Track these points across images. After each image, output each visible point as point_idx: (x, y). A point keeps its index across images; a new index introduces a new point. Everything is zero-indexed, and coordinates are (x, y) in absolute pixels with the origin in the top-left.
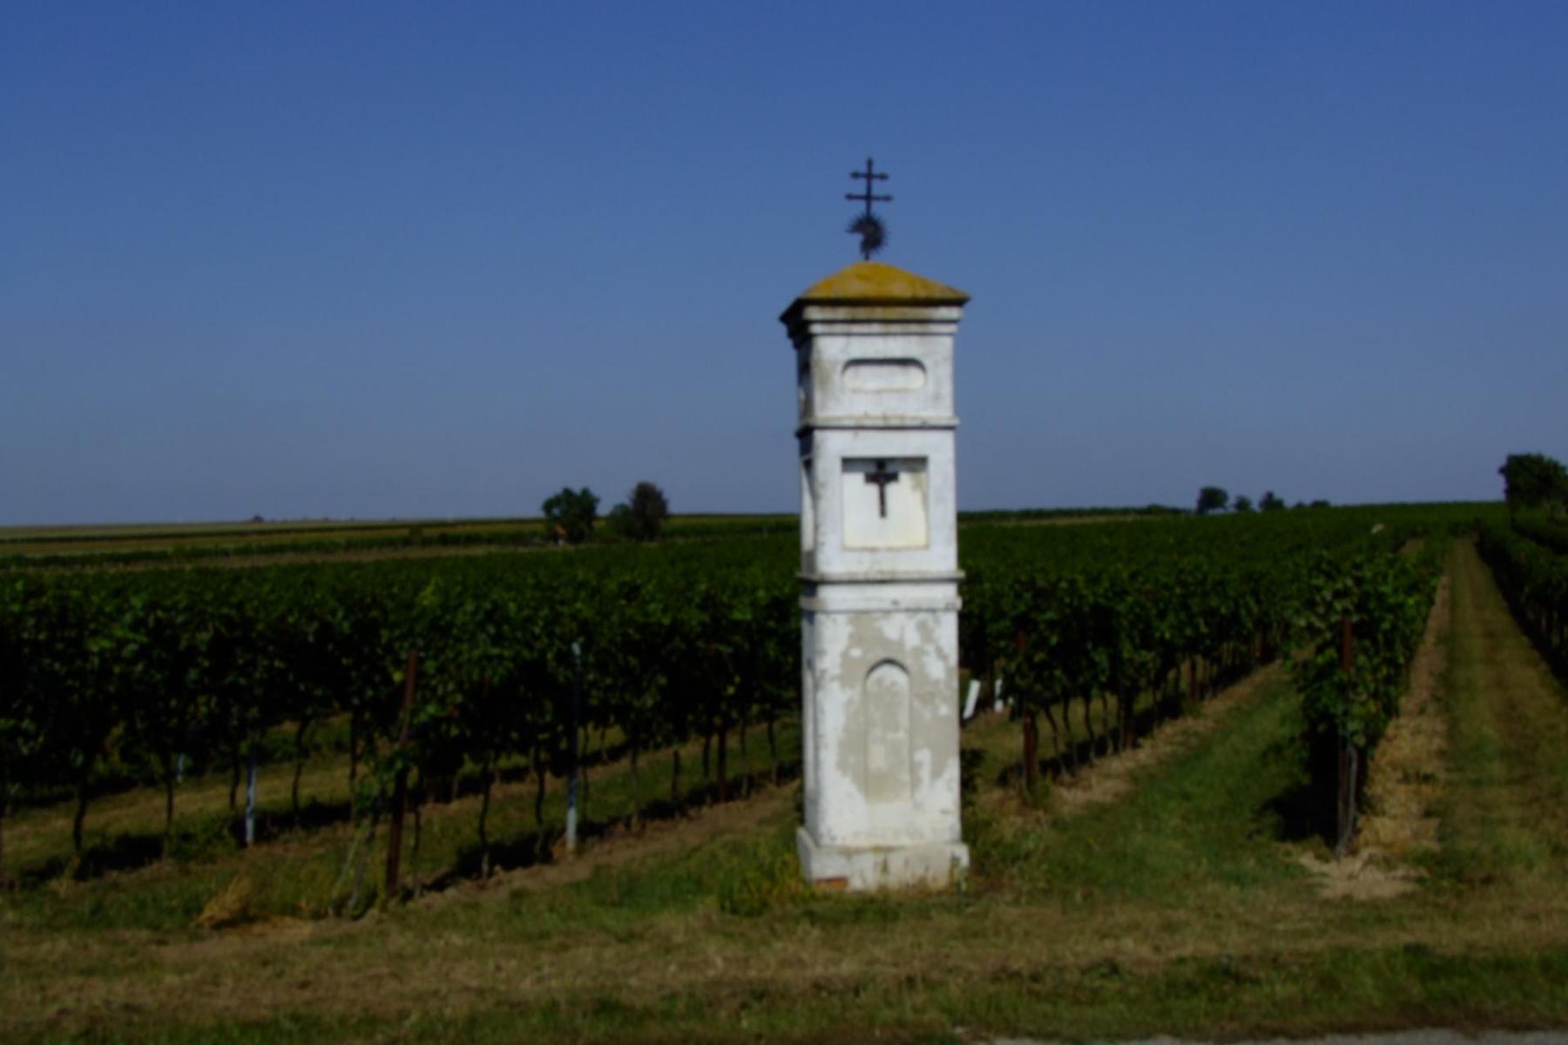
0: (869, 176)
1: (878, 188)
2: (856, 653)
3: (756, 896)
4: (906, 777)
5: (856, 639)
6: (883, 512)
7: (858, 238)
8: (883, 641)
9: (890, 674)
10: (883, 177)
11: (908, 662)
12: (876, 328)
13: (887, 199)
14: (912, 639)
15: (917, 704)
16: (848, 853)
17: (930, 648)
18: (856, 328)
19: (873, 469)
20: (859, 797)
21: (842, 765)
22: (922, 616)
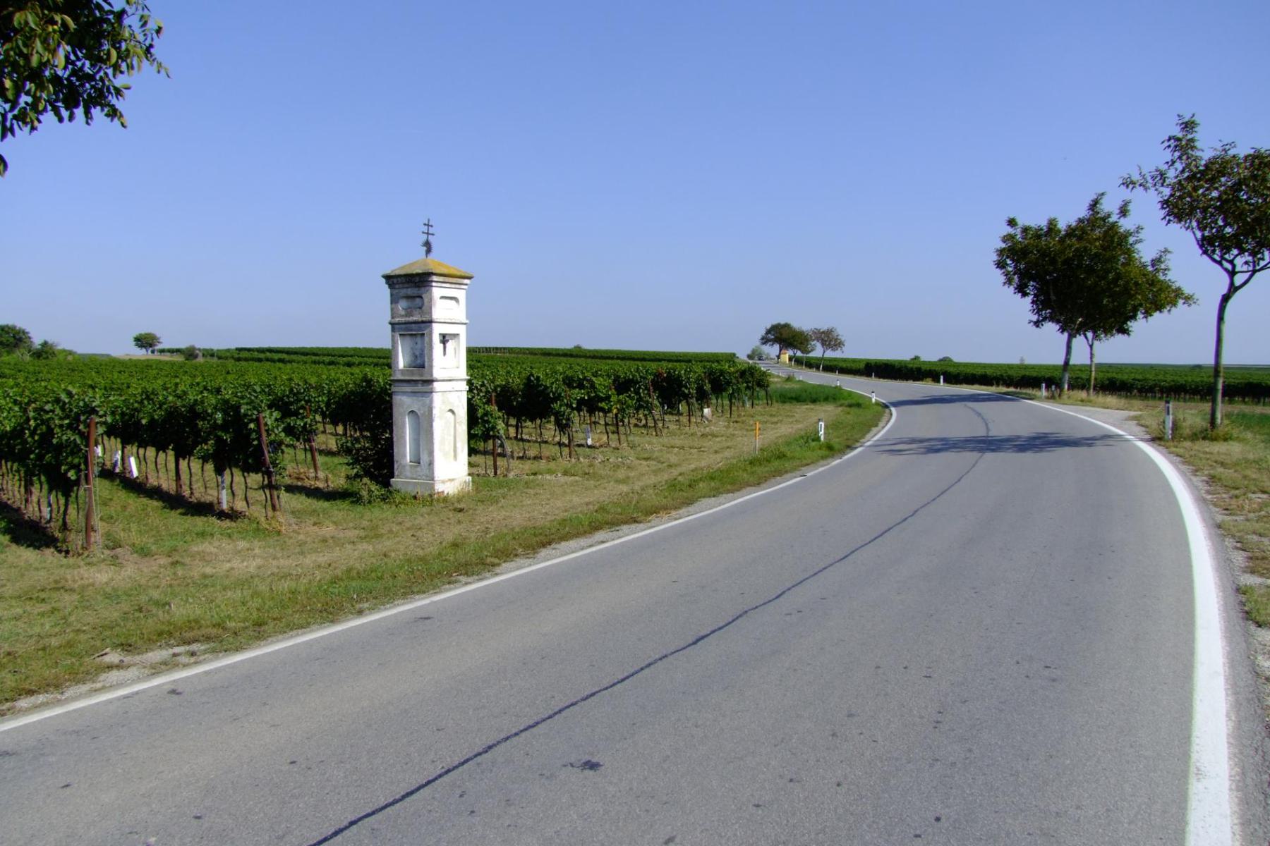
7: (425, 248)
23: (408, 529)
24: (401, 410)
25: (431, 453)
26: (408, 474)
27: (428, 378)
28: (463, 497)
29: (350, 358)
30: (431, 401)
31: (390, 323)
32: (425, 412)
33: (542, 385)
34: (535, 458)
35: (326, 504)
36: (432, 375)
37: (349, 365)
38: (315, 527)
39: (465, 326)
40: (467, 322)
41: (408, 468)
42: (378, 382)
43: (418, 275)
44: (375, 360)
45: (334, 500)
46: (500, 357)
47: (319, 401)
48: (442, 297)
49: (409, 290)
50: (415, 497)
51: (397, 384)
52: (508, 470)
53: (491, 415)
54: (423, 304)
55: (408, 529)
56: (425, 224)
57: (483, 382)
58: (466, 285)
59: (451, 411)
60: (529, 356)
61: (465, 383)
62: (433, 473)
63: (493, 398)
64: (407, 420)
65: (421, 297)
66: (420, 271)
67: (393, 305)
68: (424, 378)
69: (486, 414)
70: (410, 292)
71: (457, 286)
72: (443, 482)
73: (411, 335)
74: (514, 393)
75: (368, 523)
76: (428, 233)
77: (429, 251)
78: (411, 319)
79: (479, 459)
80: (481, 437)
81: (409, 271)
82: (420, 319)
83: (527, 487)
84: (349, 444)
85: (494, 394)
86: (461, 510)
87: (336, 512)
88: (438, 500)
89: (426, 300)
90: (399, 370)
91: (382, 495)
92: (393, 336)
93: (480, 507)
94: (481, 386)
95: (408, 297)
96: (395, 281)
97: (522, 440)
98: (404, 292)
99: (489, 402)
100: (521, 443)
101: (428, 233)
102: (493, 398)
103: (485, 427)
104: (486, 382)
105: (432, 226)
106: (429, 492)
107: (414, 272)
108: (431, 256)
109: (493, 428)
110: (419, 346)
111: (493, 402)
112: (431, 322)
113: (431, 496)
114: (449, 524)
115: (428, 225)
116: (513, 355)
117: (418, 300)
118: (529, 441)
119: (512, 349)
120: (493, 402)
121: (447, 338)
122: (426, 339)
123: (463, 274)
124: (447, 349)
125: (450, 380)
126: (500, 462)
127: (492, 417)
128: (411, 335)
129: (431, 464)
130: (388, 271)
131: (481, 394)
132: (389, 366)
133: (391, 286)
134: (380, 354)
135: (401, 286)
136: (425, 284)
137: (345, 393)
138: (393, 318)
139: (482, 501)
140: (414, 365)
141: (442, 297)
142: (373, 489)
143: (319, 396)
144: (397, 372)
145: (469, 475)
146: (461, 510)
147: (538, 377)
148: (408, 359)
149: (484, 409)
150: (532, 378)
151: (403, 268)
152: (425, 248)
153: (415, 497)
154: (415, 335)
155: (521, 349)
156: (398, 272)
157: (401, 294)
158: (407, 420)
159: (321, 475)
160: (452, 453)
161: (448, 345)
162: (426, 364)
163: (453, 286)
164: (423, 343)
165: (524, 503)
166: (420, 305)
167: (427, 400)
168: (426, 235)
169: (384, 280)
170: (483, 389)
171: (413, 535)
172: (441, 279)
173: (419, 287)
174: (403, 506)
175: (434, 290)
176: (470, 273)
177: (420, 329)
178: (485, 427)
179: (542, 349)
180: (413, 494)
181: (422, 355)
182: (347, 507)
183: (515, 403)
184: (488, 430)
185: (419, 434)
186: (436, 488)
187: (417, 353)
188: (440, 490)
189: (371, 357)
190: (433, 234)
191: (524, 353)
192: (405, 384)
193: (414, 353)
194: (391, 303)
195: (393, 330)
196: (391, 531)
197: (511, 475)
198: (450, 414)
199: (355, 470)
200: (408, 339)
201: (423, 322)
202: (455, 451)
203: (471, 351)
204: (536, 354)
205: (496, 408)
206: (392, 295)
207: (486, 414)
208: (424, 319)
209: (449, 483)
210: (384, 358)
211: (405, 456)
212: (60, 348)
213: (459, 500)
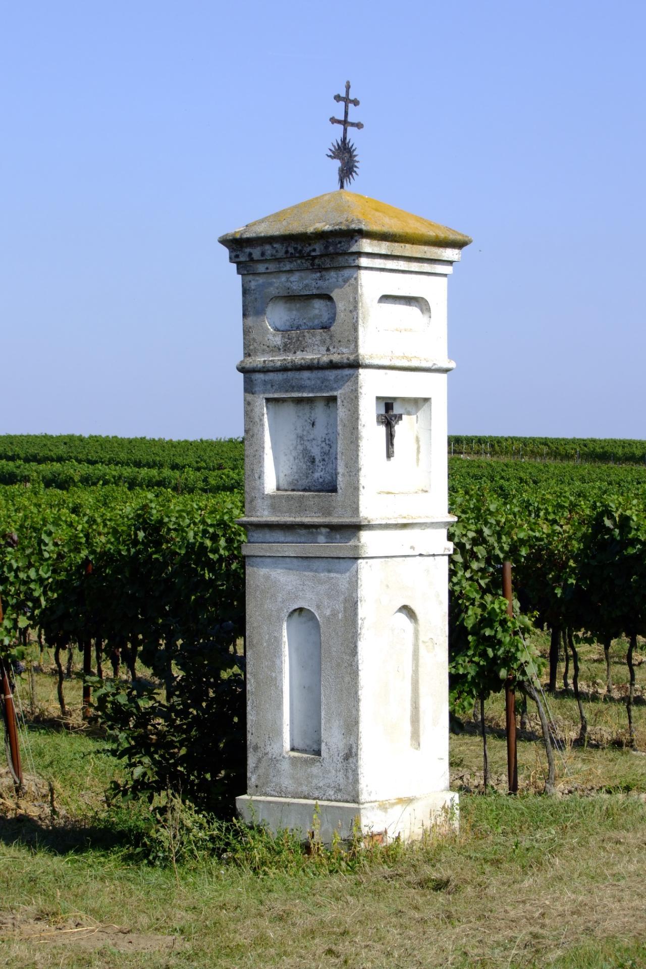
7: (337, 163)
10: (333, 120)
23: (311, 933)
24: (269, 605)
25: (351, 726)
26: (287, 783)
27: (346, 520)
28: (440, 847)
29: (57, 466)
30: (354, 584)
31: (242, 369)
32: (334, 614)
33: (637, 540)
34: (617, 744)
35: (59, 863)
36: (356, 510)
37: (64, 484)
38: (41, 925)
39: (444, 377)
40: (452, 365)
41: (285, 766)
42: (180, 529)
43: (321, 236)
44: (127, 471)
45: (79, 851)
46: (470, 465)
47: (25, 583)
48: (386, 298)
49: (295, 277)
50: (307, 848)
51: (257, 535)
52: (549, 777)
53: (503, 623)
54: (333, 319)
55: (311, 933)
56: (338, 98)
57: (480, 532)
58: (450, 263)
59: (407, 610)
60: (548, 461)
61: (444, 533)
62: (356, 781)
63: (509, 577)
64: (285, 633)
65: (329, 298)
66: (327, 228)
67: (250, 321)
68: (334, 520)
69: (488, 620)
70: (298, 282)
71: (426, 267)
72: (384, 807)
73: (299, 401)
74: (555, 563)
75: (190, 916)
76: (345, 123)
77: (347, 171)
78: (299, 357)
79: (472, 744)
80: (473, 682)
81: (296, 227)
82: (325, 359)
83: (614, 827)
84: (122, 699)
85: (509, 565)
86: (440, 885)
87: (95, 885)
88: (370, 856)
89: (341, 306)
90: (264, 497)
91: (212, 839)
92: (248, 403)
93: (495, 883)
94: (475, 542)
95: (291, 298)
96: (256, 253)
97: (578, 695)
98: (280, 283)
99: (496, 586)
100: (573, 704)
101: (345, 123)
102: (509, 577)
103: (484, 655)
104: (487, 531)
105: (356, 103)
106: (345, 834)
107: (310, 230)
108: (354, 185)
109: (509, 659)
110: (320, 431)
111: (509, 586)
112: (355, 365)
113: (349, 844)
114: (423, 921)
115: (347, 100)
116: (504, 459)
117: (318, 306)
118: (594, 698)
119: (499, 441)
120: (509, 586)
121: (397, 410)
122: (342, 412)
123: (442, 235)
124: (396, 441)
125: (404, 526)
126: (528, 754)
127: (505, 630)
128: (299, 401)
129: (350, 755)
130: (236, 227)
131: (475, 565)
132: (235, 487)
133: (244, 267)
134: (138, 455)
135: (272, 267)
136: (341, 260)
137: (86, 561)
138: (247, 355)
139: (496, 863)
140: (305, 482)
141: (386, 298)
142: (189, 823)
143: (30, 566)
144: (259, 502)
145: (452, 787)
146: (440, 885)
147: (626, 520)
148: (287, 468)
149: (483, 606)
150: (608, 523)
151: (277, 216)
152: (337, 163)
153: (307, 848)
154: (310, 400)
155: (525, 441)
156: (263, 230)
157: (273, 291)
158: (285, 633)
159: (30, 780)
160: (408, 728)
161: (398, 428)
162: (341, 482)
163: (415, 266)
164: (332, 424)
165: (619, 868)
166: (325, 318)
167: (342, 580)
168: (340, 127)
169: (225, 252)
170: (481, 551)
171: (330, 952)
172: (383, 248)
173: (321, 269)
174: (272, 871)
175: (364, 275)
176: (459, 231)
177: (325, 384)
178: (484, 655)
179: (584, 443)
180: (302, 838)
181: (329, 455)
182: (118, 873)
183: (559, 592)
184: (494, 664)
185: (317, 672)
186: (364, 821)
187: (316, 452)
188: (376, 829)
189: (110, 462)
190: (359, 126)
191: (533, 454)
192: (279, 535)
193: (305, 452)
194: (245, 315)
195: (249, 388)
196: (261, 940)
197: (558, 790)
198: (403, 617)
199: (138, 771)
200: (289, 412)
201: (333, 366)
202: (415, 720)
203: (456, 444)
204: (567, 457)
205: (517, 604)
206: (245, 292)
207: (488, 620)
208: (336, 358)
209: (398, 808)
210: (150, 466)
211: (279, 733)
212: (111, 436)
213: (431, 858)
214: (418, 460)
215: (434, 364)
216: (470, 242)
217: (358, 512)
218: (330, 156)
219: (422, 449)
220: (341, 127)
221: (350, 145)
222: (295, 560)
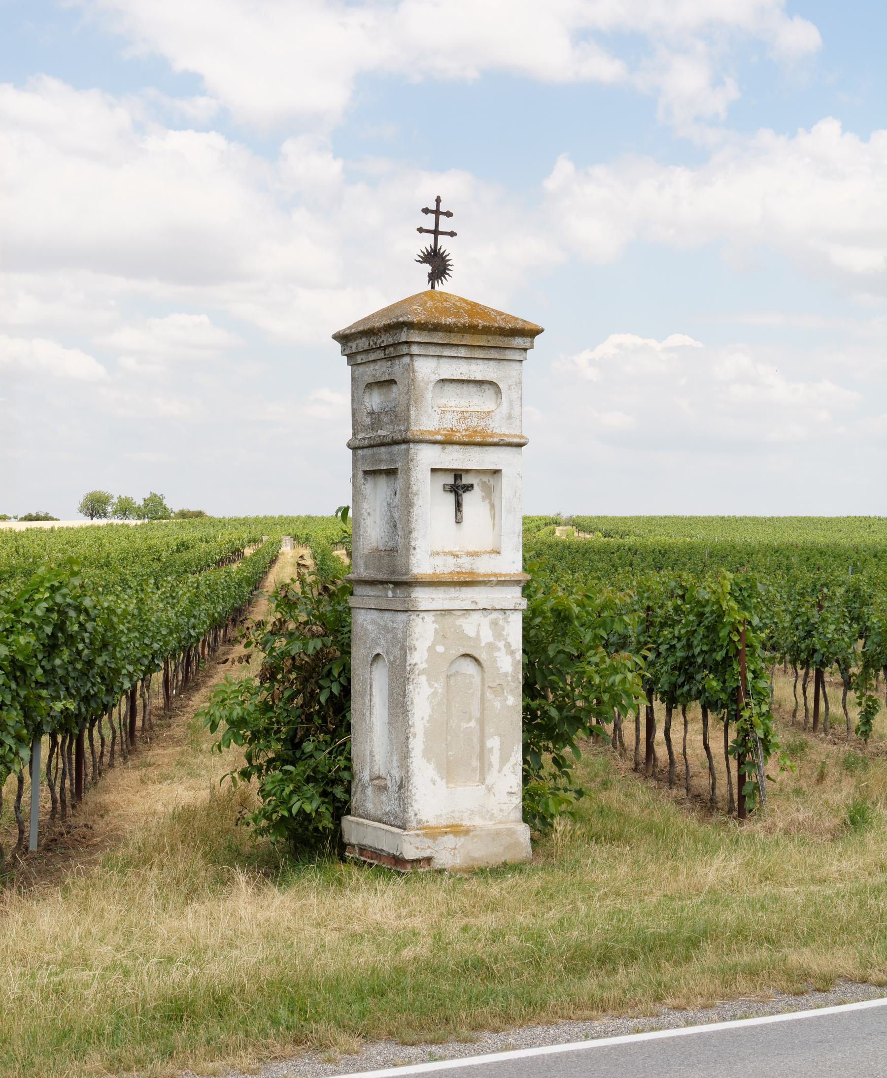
0: (437, 212)
1: (445, 224)
2: (440, 649)
3: (705, 859)
4: (475, 763)
5: (441, 636)
6: (458, 521)
7: (427, 268)
8: (462, 636)
9: (468, 667)
10: (449, 214)
11: (482, 657)
12: (463, 352)
13: (452, 234)
14: (487, 636)
15: (489, 695)
16: (433, 833)
17: (501, 644)
18: (447, 352)
19: (450, 480)
20: (441, 783)
21: (427, 754)
22: (495, 615)
101: (436, 232)
108: (445, 286)
152: (427, 268)
169: (338, 346)
214: (494, 524)
215: (502, 440)
216: (542, 331)
217: (524, 619)
218: (419, 261)
219: (496, 515)
220: (432, 236)
221: (442, 251)
222: (375, 611)
